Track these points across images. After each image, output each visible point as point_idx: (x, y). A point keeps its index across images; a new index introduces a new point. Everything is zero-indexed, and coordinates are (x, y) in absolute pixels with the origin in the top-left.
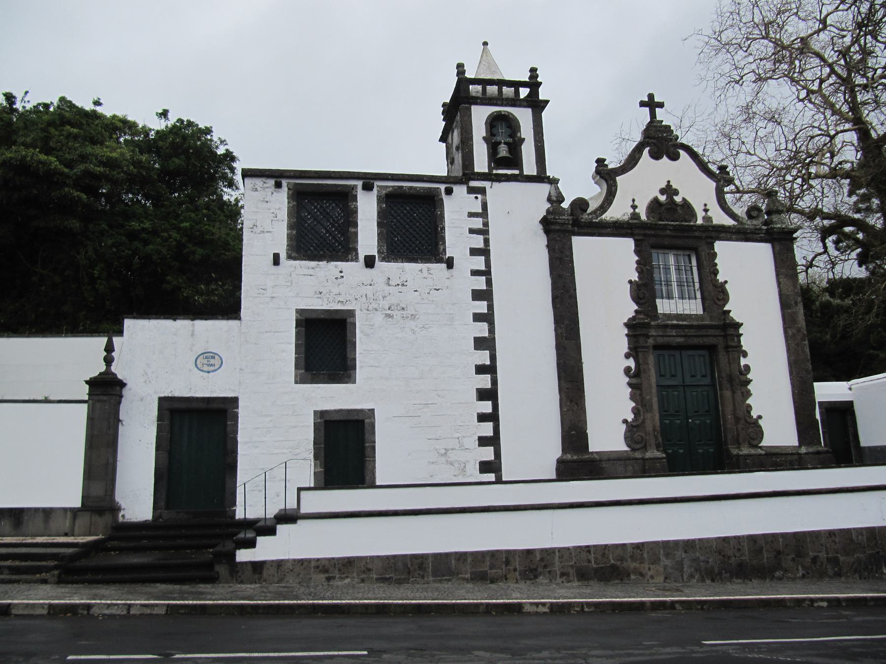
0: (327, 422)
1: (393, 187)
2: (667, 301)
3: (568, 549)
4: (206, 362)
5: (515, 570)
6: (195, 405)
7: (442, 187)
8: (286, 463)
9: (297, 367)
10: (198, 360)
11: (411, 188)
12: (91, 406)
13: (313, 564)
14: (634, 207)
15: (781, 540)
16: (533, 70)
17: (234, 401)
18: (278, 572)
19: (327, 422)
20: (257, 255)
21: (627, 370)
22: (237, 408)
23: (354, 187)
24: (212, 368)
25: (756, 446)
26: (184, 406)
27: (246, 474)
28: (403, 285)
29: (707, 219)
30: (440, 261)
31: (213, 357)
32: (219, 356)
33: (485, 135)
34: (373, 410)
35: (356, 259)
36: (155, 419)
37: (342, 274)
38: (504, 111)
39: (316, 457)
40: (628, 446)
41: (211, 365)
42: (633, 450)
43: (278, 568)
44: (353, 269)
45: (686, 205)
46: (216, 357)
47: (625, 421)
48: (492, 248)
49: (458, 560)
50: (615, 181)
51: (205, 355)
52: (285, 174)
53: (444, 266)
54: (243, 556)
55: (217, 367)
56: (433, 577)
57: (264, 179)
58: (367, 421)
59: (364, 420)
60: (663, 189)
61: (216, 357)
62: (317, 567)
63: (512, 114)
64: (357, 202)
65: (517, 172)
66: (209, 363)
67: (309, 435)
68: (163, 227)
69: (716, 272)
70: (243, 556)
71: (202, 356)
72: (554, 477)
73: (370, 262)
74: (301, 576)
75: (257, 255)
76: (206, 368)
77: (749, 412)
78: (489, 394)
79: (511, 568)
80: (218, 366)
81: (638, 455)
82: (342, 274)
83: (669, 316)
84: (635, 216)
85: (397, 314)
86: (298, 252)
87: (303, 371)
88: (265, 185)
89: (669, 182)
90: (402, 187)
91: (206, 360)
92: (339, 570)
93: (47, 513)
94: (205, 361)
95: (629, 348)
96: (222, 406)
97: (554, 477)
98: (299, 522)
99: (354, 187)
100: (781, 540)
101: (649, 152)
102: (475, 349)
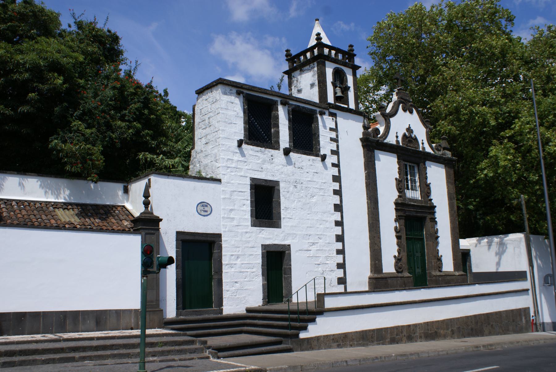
0: (268, 252)
1: (295, 105)
2: (415, 192)
3: (421, 324)
4: (203, 209)
5: (405, 336)
6: (197, 238)
7: (318, 110)
8: (314, 279)
9: (252, 216)
10: (198, 207)
11: (303, 107)
12: (144, 237)
13: (332, 338)
14: (397, 137)
15: (483, 317)
16: (351, 46)
17: (219, 236)
18: (318, 343)
19: (268, 252)
20: (228, 139)
21: (396, 228)
22: (221, 242)
23: (276, 102)
24: (206, 214)
25: (441, 271)
26: (191, 238)
27: (227, 285)
28: (301, 168)
29: (424, 148)
30: (317, 155)
31: (206, 206)
32: (211, 206)
33: (332, 81)
34: (289, 245)
35: (278, 148)
36: (175, 246)
37: (272, 158)
38: (340, 68)
39: (263, 275)
40: (396, 270)
41: (206, 211)
42: (398, 272)
43: (318, 341)
44: (279, 155)
45: (416, 139)
46: (208, 205)
47: (395, 257)
48: (340, 151)
49: (385, 331)
50: (389, 120)
51: (202, 204)
52: (244, 86)
53: (319, 159)
54: (303, 335)
55: (209, 213)
56: (377, 341)
57: (230, 87)
58: (287, 252)
59: (285, 252)
60: (117, 43)
61: (208, 205)
62: (333, 339)
63: (343, 70)
64: (278, 111)
65: (346, 106)
66: (204, 209)
67: (259, 261)
68: (496, 185)
69: (426, 178)
70: (303, 335)
71: (200, 205)
72: (367, 289)
73: (287, 152)
74: (327, 345)
75: (228, 139)
76: (203, 213)
77: (438, 253)
78: (340, 238)
79: (403, 335)
80: (210, 212)
81: (400, 275)
82: (272, 158)
83: (410, 200)
84: (398, 142)
85: (299, 186)
86: (249, 139)
87: (255, 219)
88: (231, 92)
89: (409, 125)
90: (299, 106)
91: (203, 207)
92: (342, 340)
93: (118, 313)
94: (202, 208)
95: (396, 216)
96: (212, 239)
97: (367, 289)
98: (325, 314)
99: (276, 102)
100: (483, 317)
101: (402, 106)
102: (335, 211)
